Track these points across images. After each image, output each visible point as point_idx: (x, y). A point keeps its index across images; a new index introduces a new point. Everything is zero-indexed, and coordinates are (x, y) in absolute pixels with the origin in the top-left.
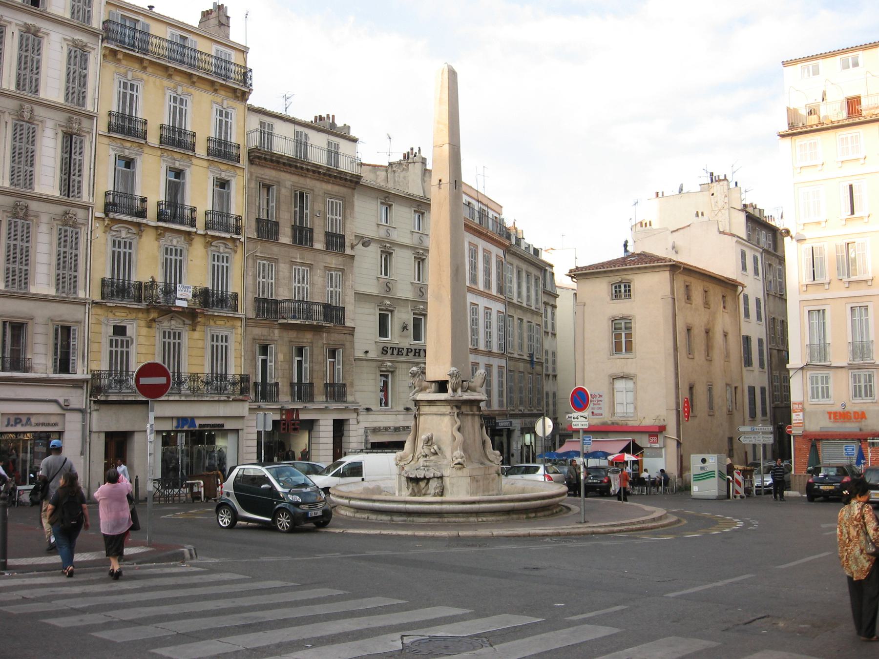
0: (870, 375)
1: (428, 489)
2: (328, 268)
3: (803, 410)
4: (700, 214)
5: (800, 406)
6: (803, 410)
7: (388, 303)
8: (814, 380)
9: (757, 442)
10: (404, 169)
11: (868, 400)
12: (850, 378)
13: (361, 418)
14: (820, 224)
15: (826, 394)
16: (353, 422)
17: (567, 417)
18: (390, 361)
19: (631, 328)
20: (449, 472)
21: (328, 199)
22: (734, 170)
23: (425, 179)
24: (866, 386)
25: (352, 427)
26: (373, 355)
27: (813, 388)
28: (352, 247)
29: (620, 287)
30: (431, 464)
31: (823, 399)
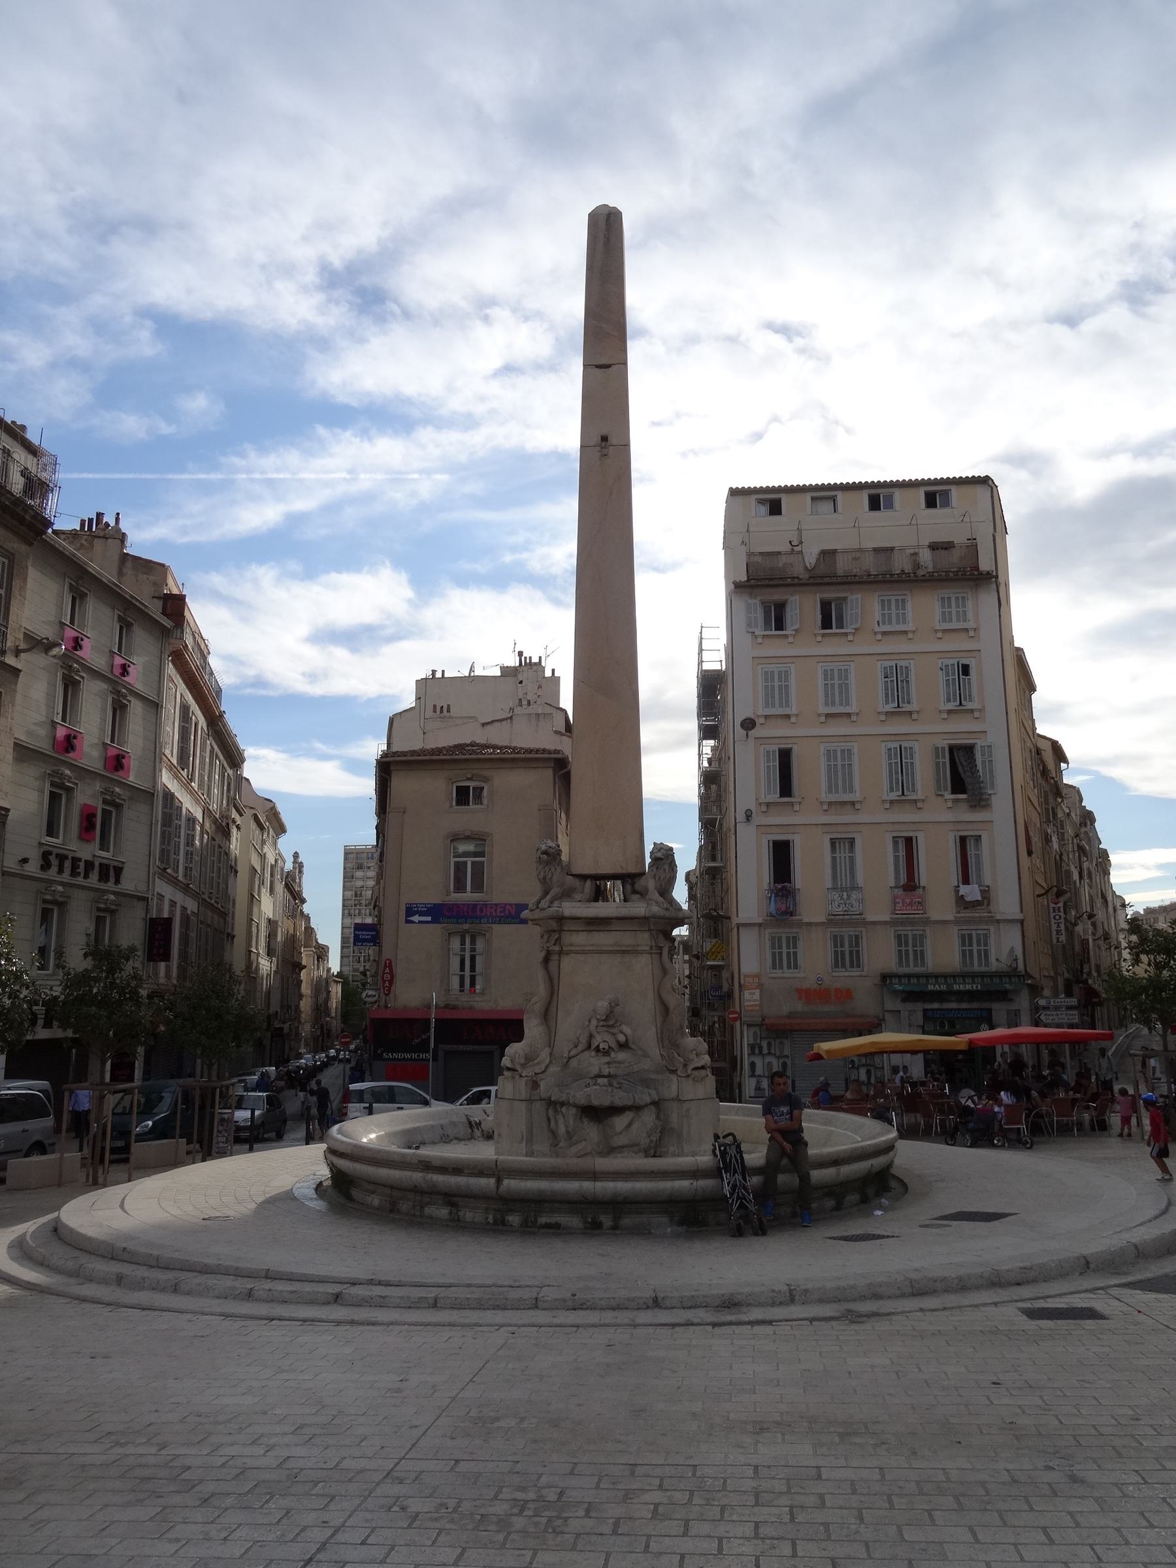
0: (857, 937)
4: (525, 702)
9: (1060, 1021)
10: (82, 545)
11: (855, 973)
12: (829, 941)
14: (790, 718)
15: (794, 964)
22: (548, 654)
23: (125, 570)
24: (851, 952)
26: (33, 868)
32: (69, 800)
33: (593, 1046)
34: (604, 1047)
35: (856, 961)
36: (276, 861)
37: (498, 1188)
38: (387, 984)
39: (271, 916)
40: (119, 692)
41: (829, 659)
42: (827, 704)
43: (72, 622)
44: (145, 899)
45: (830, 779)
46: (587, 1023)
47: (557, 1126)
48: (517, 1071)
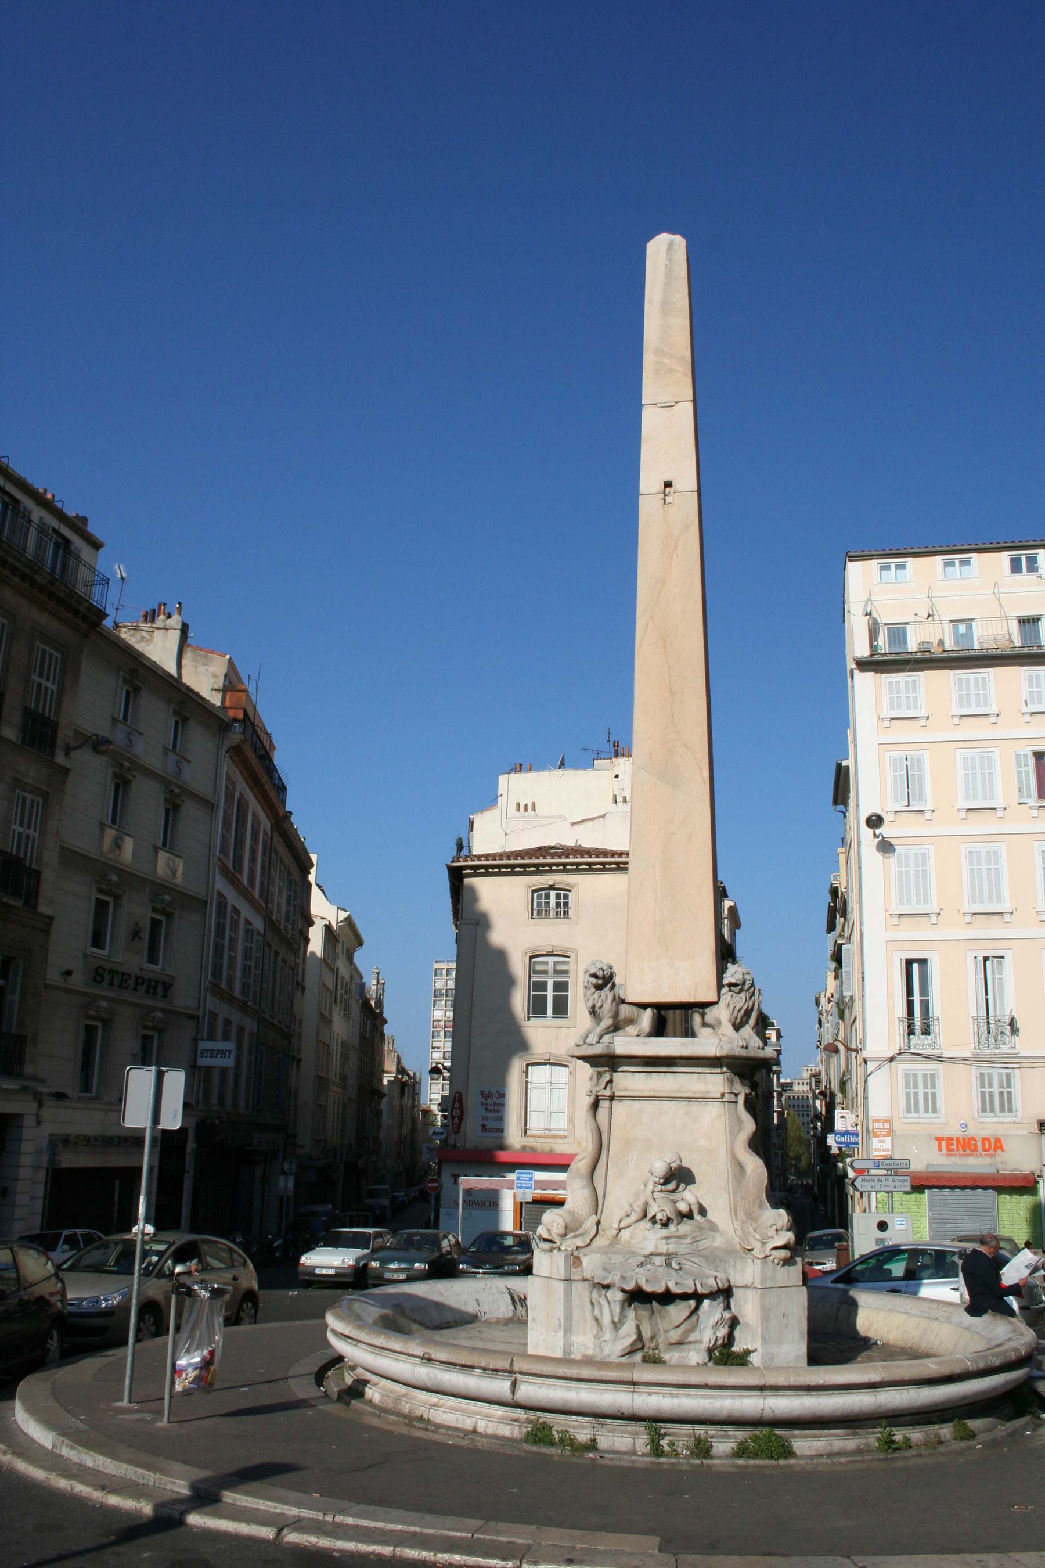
0: (1008, 1075)
1: (692, 1330)
2: (17, 783)
3: (890, 1132)
4: (620, 799)
5: (887, 1126)
6: (890, 1132)
7: (115, 878)
8: (910, 1080)
11: (1006, 1117)
13: (46, 1113)
16: (29, 1121)
17: (431, 1132)
18: (106, 998)
19: (566, 972)
20: (749, 1271)
21: (38, 643)
24: (1001, 1093)
25: (27, 1133)
26: (77, 981)
27: (908, 1094)
28: (68, 750)
29: (547, 896)
30: (683, 1248)
31: (927, 1115)
32: (116, 907)
33: (649, 1216)
34: (661, 1218)
35: (1007, 1103)
36: (351, 977)
37: (513, 1393)
38: (456, 1120)
39: (345, 1038)
40: (172, 791)
41: (968, 744)
42: (967, 798)
43: (125, 718)
44: (195, 1018)
45: (973, 888)
46: (643, 1187)
47: (602, 1314)
48: (555, 1243)
